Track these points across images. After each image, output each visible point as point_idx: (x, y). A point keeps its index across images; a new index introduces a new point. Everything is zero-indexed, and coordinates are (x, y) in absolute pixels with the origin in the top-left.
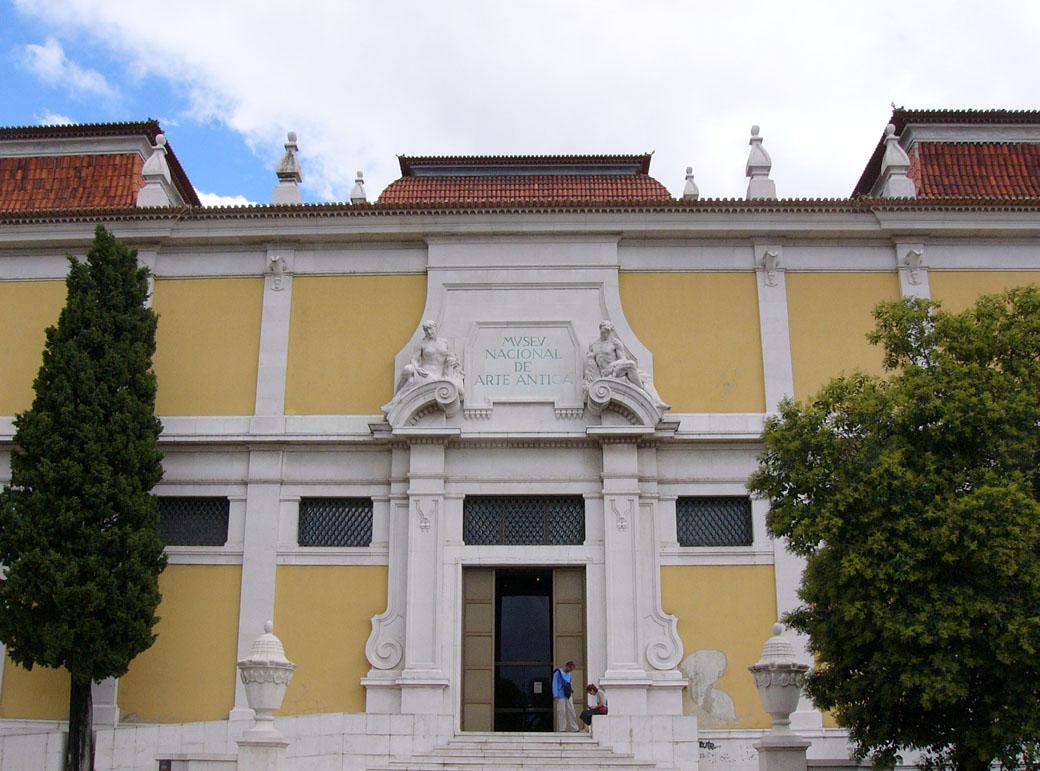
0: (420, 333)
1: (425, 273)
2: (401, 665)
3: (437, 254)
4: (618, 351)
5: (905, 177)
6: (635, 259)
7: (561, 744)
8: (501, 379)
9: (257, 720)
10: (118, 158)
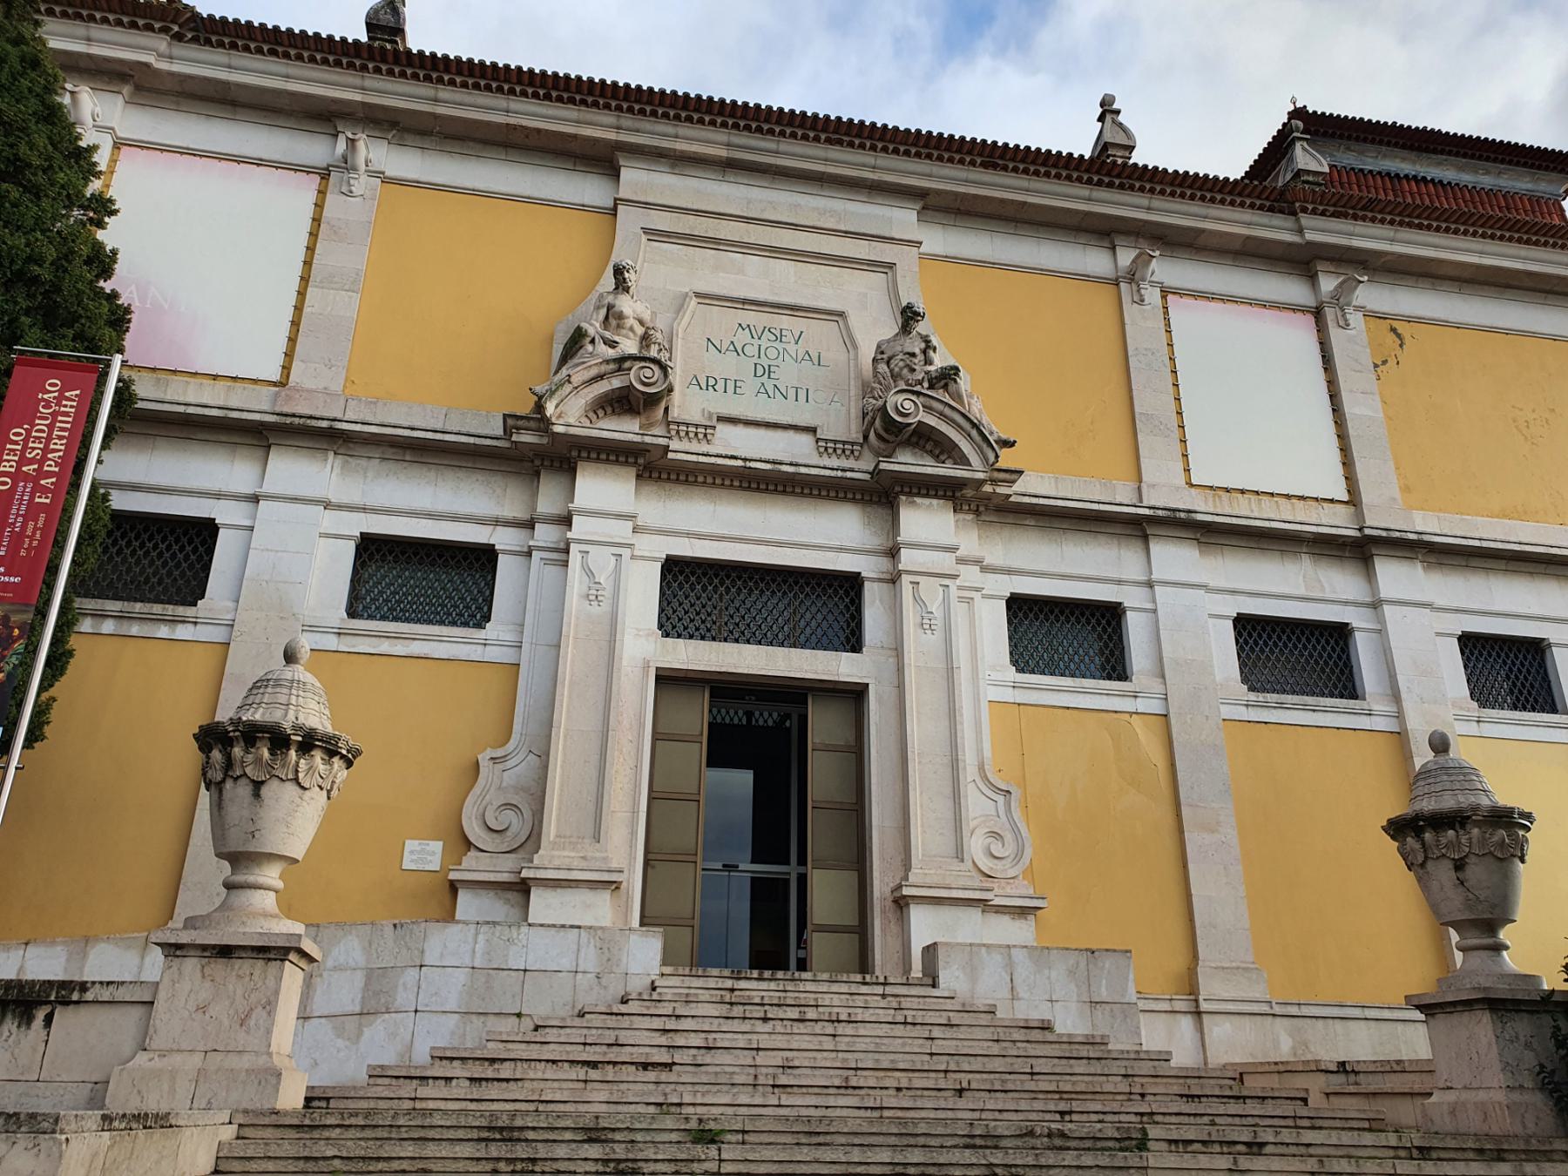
0: (608, 281)
1: (613, 212)
2: (533, 839)
3: (635, 178)
6: (939, 239)
8: (731, 385)
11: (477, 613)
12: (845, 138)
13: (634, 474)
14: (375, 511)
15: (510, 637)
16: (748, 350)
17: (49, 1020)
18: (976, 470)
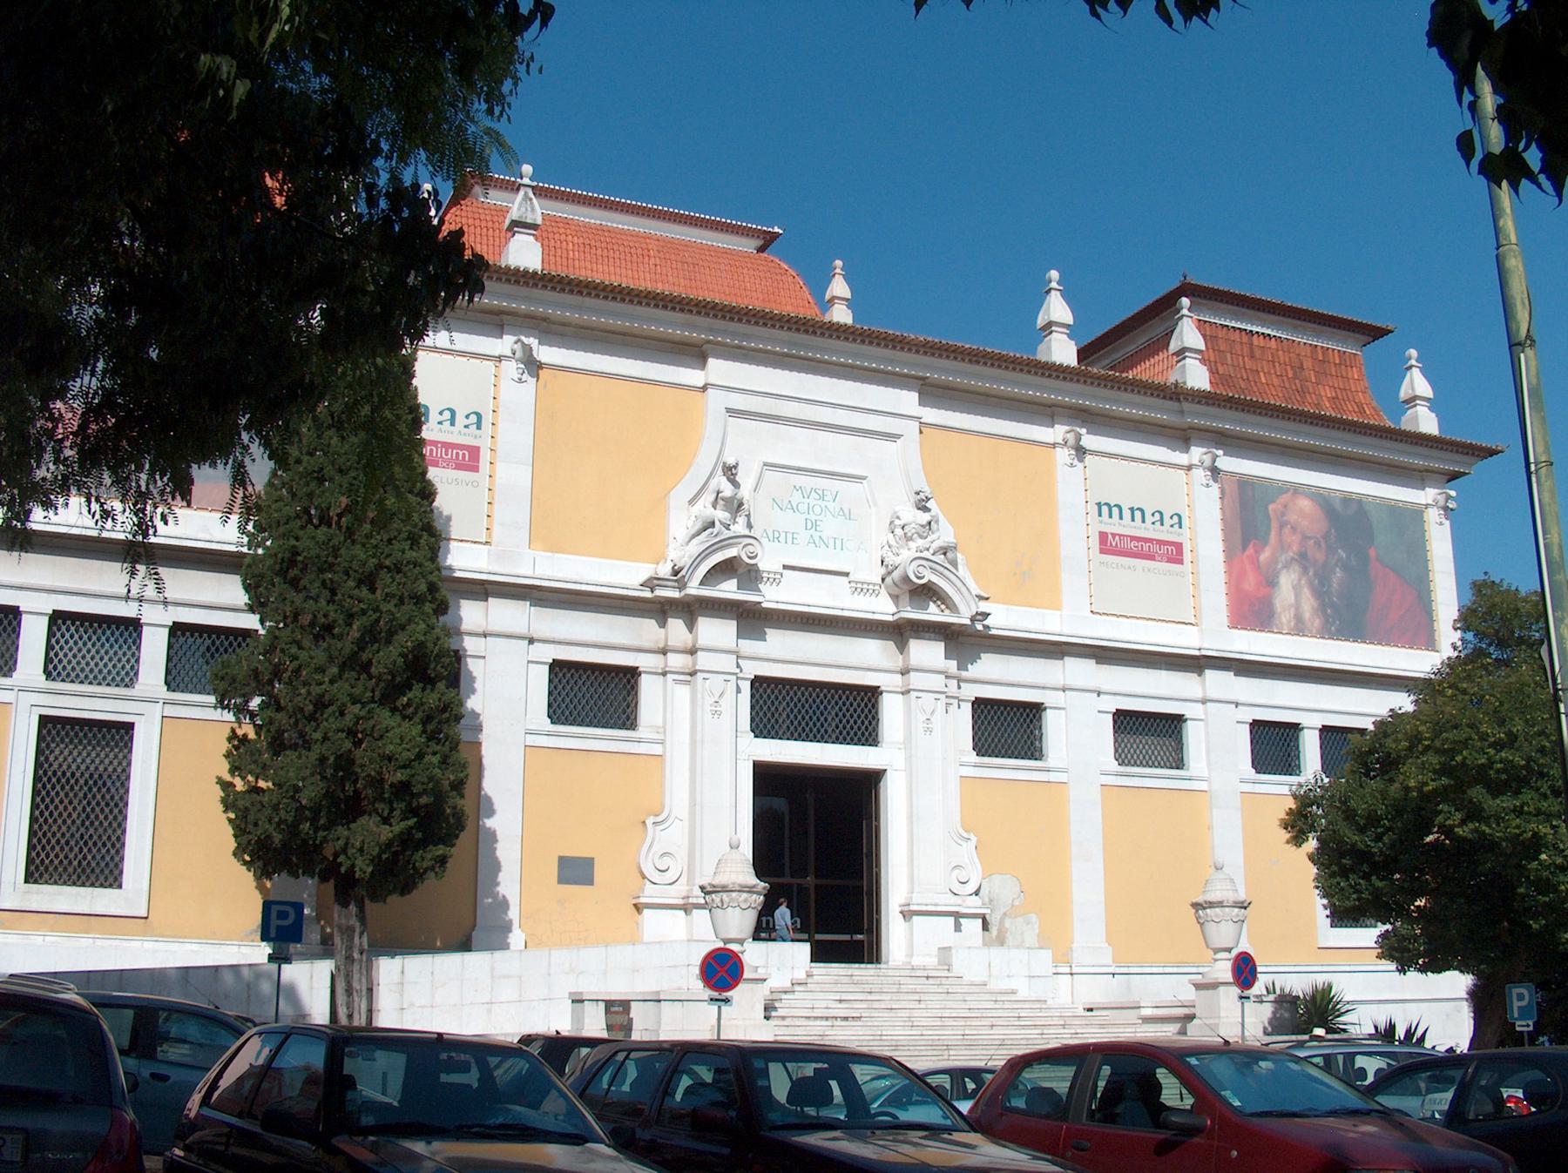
5: (1065, 336)
6: (932, 415)
7: (928, 977)
8: (790, 536)
9: (1216, 960)
16: (803, 508)
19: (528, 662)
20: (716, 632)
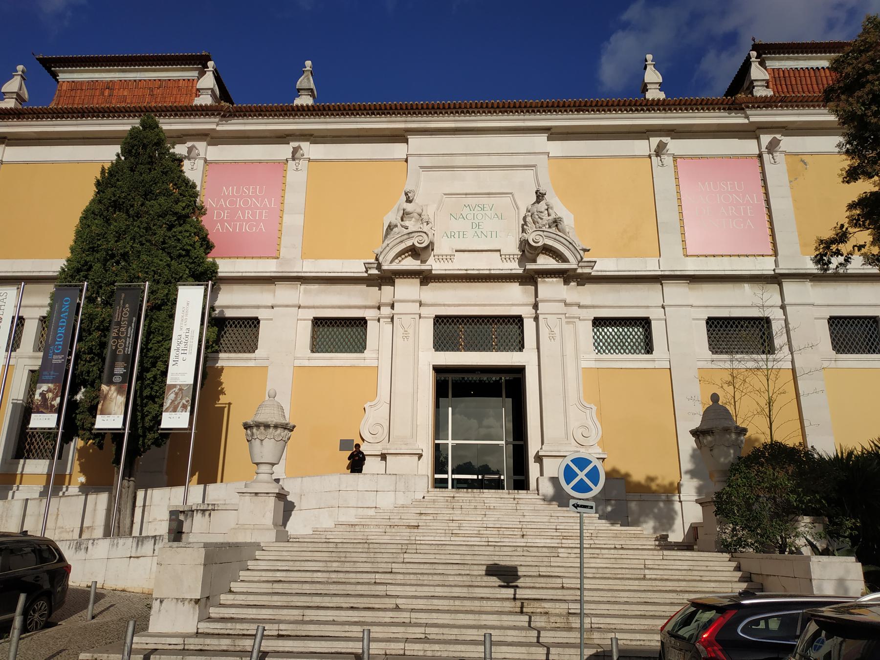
4: (550, 210)
6: (558, 148)
8: (461, 234)
10: (181, 82)
11: (360, 346)
12: (508, 109)
13: (419, 282)
14: (318, 307)
15: (375, 356)
17: (210, 515)
18: (572, 264)
19: (298, 320)
20: (406, 289)
